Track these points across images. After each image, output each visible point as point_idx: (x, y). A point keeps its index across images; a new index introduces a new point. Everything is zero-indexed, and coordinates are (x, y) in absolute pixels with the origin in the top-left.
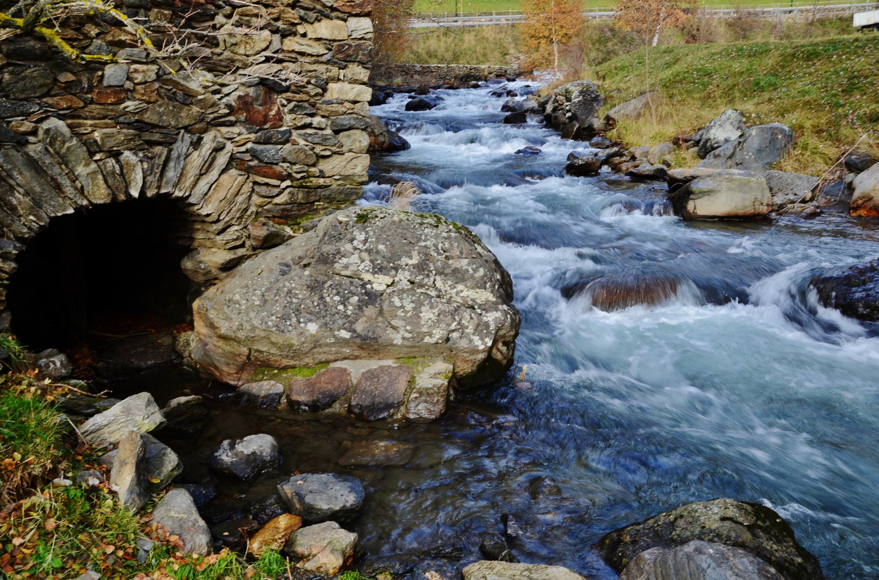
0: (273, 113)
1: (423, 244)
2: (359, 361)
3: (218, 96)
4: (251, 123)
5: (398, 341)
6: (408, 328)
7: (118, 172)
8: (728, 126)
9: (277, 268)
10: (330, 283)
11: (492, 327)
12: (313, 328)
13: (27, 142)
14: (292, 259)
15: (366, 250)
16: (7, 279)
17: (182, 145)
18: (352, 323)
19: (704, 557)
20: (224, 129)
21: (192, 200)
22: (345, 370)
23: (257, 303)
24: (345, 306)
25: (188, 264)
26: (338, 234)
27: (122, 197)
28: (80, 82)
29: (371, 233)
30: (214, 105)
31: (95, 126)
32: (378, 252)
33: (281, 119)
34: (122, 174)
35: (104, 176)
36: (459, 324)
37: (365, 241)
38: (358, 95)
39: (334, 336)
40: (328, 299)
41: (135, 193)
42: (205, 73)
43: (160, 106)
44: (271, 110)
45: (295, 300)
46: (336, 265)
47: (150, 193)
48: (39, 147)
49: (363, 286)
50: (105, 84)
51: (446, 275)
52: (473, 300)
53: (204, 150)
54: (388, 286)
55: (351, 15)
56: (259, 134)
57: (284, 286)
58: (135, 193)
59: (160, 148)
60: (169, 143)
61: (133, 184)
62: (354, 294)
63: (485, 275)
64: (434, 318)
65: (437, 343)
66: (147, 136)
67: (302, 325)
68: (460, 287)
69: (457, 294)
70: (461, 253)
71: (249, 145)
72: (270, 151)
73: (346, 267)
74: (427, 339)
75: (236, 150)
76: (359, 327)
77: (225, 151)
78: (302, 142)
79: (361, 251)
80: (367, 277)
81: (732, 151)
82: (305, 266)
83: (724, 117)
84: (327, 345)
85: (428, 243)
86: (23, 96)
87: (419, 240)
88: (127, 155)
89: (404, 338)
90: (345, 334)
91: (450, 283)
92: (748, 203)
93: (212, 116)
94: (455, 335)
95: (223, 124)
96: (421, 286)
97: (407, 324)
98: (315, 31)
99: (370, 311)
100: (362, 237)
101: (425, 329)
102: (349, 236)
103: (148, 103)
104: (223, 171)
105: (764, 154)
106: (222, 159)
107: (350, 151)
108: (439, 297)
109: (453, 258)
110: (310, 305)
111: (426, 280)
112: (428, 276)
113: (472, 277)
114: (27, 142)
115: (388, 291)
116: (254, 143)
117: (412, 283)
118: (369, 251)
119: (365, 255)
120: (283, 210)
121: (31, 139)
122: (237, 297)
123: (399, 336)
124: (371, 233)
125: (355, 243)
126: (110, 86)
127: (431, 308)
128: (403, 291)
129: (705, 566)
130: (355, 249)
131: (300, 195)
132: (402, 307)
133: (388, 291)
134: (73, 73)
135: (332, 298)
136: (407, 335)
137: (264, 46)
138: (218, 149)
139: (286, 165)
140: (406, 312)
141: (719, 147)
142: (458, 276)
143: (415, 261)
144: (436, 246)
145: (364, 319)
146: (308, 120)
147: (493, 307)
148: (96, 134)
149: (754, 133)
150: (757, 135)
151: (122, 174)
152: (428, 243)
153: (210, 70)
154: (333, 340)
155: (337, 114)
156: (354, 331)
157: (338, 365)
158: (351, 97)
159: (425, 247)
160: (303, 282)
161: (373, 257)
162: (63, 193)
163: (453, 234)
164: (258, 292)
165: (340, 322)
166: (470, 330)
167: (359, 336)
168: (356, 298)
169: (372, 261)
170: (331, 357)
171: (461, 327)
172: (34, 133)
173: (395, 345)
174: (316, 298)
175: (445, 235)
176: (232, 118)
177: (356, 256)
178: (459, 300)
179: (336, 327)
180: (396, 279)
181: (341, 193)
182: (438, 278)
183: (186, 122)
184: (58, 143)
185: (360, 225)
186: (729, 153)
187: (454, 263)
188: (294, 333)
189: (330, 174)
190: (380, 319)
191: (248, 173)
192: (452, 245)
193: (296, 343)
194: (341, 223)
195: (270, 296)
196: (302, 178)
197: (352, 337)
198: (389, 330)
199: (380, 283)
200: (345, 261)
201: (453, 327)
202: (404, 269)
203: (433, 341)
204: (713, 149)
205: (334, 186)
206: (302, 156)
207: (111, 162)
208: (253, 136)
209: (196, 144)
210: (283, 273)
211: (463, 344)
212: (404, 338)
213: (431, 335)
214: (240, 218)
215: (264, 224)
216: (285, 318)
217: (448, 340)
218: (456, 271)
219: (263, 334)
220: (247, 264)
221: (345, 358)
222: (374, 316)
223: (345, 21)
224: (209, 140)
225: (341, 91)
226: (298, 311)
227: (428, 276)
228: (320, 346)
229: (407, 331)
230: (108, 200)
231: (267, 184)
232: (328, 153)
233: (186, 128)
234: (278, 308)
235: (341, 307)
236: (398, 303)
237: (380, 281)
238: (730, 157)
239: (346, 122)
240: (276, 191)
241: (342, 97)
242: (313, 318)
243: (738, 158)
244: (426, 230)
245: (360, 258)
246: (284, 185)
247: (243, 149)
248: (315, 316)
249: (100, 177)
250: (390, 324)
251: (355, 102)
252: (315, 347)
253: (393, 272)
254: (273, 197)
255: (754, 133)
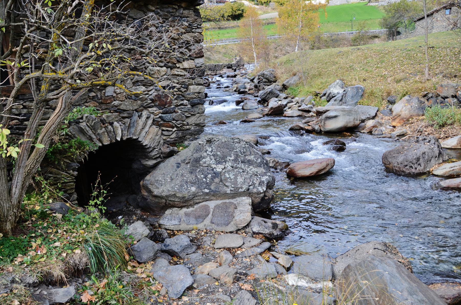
0: (169, 100)
1: (235, 151)
2: (212, 201)
3: (147, 96)
4: (159, 107)
5: (229, 192)
6: (233, 186)
7: (112, 131)
8: (338, 87)
9: (175, 165)
10: (199, 170)
11: (265, 183)
12: (193, 189)
13: (80, 122)
14: (181, 161)
15: (212, 155)
16: (75, 179)
17: (135, 117)
18: (209, 186)
19: (375, 261)
20: (150, 109)
21: (140, 139)
22: (207, 205)
23: (169, 180)
24: (206, 179)
25: (135, 166)
26: (199, 149)
27: (114, 141)
28: (97, 96)
29: (214, 148)
30: (146, 99)
31: (103, 113)
32: (217, 155)
33: (172, 103)
34: (114, 132)
35: (107, 133)
36: (253, 182)
37: (212, 151)
38: (200, 90)
39: (202, 192)
40: (199, 177)
41: (119, 139)
42: (142, 87)
43: (126, 102)
44: (167, 99)
45: (185, 178)
46: (201, 162)
47: (125, 138)
48: (84, 124)
49: (213, 170)
50: (106, 95)
51: (245, 163)
52: (257, 172)
53: (143, 118)
54: (223, 169)
55: (196, 58)
56: (164, 109)
57: (180, 173)
58: (119, 139)
59: (127, 119)
60: (130, 117)
61: (118, 135)
62: (209, 174)
63: (261, 161)
64: (243, 181)
65: (244, 191)
66: (122, 115)
67: (189, 188)
68: (251, 167)
69: (250, 170)
70: (251, 153)
71: (160, 115)
72: (168, 117)
73: (205, 163)
74: (240, 190)
75: (155, 117)
76: (212, 187)
77: (151, 118)
78: (180, 112)
79: (210, 155)
80: (214, 166)
81: (341, 98)
82: (187, 163)
83: (335, 83)
84: (199, 196)
85: (237, 150)
86: (78, 104)
87: (234, 149)
88: (115, 123)
89: (231, 190)
90: (207, 191)
91: (247, 166)
92: (352, 120)
93: (145, 104)
94: (251, 187)
95: (150, 107)
96: (236, 168)
97: (232, 184)
98: (183, 66)
99: (217, 180)
100: (210, 150)
101: (239, 186)
102: (205, 149)
103: (122, 101)
104: (151, 126)
105: (354, 98)
106: (150, 122)
107: (198, 113)
108: (243, 172)
109: (247, 155)
110: (192, 180)
111: (238, 165)
112: (239, 164)
113: (256, 162)
114: (80, 122)
115: (224, 171)
116: (162, 114)
117: (233, 167)
118: (214, 155)
119: (212, 157)
120: (175, 140)
121: (81, 121)
122: (160, 179)
123: (229, 190)
124: (214, 148)
125: (208, 152)
126: (108, 96)
127: (241, 177)
128: (229, 171)
129: (376, 264)
130: (208, 155)
131: (180, 134)
132: (230, 177)
133: (224, 171)
134: (94, 92)
135: (200, 176)
136: (232, 189)
137: (164, 73)
138: (148, 118)
139: (174, 122)
140: (231, 179)
141: (335, 96)
142: (250, 163)
143: (232, 158)
144: (240, 151)
145: (214, 184)
146: (182, 102)
147: (265, 174)
148: (104, 116)
149: (349, 90)
150: (351, 90)
151: (114, 132)
152: (237, 150)
153: (144, 85)
154: (202, 194)
155: (193, 98)
156: (210, 189)
157: (204, 203)
158: (197, 91)
159: (236, 151)
160: (188, 170)
161: (215, 158)
162: (93, 141)
163: (247, 146)
164: (169, 176)
165: (205, 185)
166: (257, 185)
167: (212, 191)
168: (210, 175)
169: (215, 159)
170: (201, 201)
171: (254, 184)
172: (82, 118)
173: (228, 193)
174: (194, 177)
175: (244, 146)
176: (153, 104)
177: (209, 158)
178: (251, 172)
179: (203, 188)
180: (226, 166)
181: (195, 131)
182: (242, 164)
183: (136, 108)
184: (90, 121)
185: (208, 144)
186: (340, 98)
187: (248, 158)
188: (186, 192)
189: (191, 124)
190: (221, 183)
191: (160, 126)
192: (247, 150)
193: (187, 196)
194: (200, 144)
195: (174, 177)
196: (181, 126)
197: (210, 192)
198: (225, 187)
199: (219, 168)
200: (204, 160)
201: (250, 184)
202: (228, 162)
203: (243, 190)
204: (333, 97)
205: (193, 129)
206: (180, 117)
207: (110, 127)
208: (161, 111)
209: (140, 117)
210: (178, 167)
211: (255, 190)
212: (231, 190)
213: (242, 188)
214: (158, 145)
215: (168, 147)
216: (182, 186)
217: (249, 189)
218: (249, 161)
219: (173, 193)
220: (162, 165)
221: (207, 201)
222: (218, 182)
223: (194, 60)
224: (145, 113)
225: (194, 89)
226: (187, 182)
227: (239, 164)
228: (197, 196)
229: (232, 187)
230: (109, 143)
231: (167, 130)
232: (190, 115)
233: (136, 110)
234: (178, 182)
235: (204, 180)
236: (227, 176)
237: (219, 167)
238: (341, 101)
239: (196, 102)
240: (171, 133)
241: (194, 91)
242: (193, 185)
243: (344, 100)
244: (236, 145)
245: (210, 158)
246: (174, 130)
247: (158, 116)
248: (193, 183)
249: (106, 133)
250: (225, 185)
251: (199, 93)
252: (194, 197)
253: (224, 163)
254: (170, 135)
255: (349, 90)
